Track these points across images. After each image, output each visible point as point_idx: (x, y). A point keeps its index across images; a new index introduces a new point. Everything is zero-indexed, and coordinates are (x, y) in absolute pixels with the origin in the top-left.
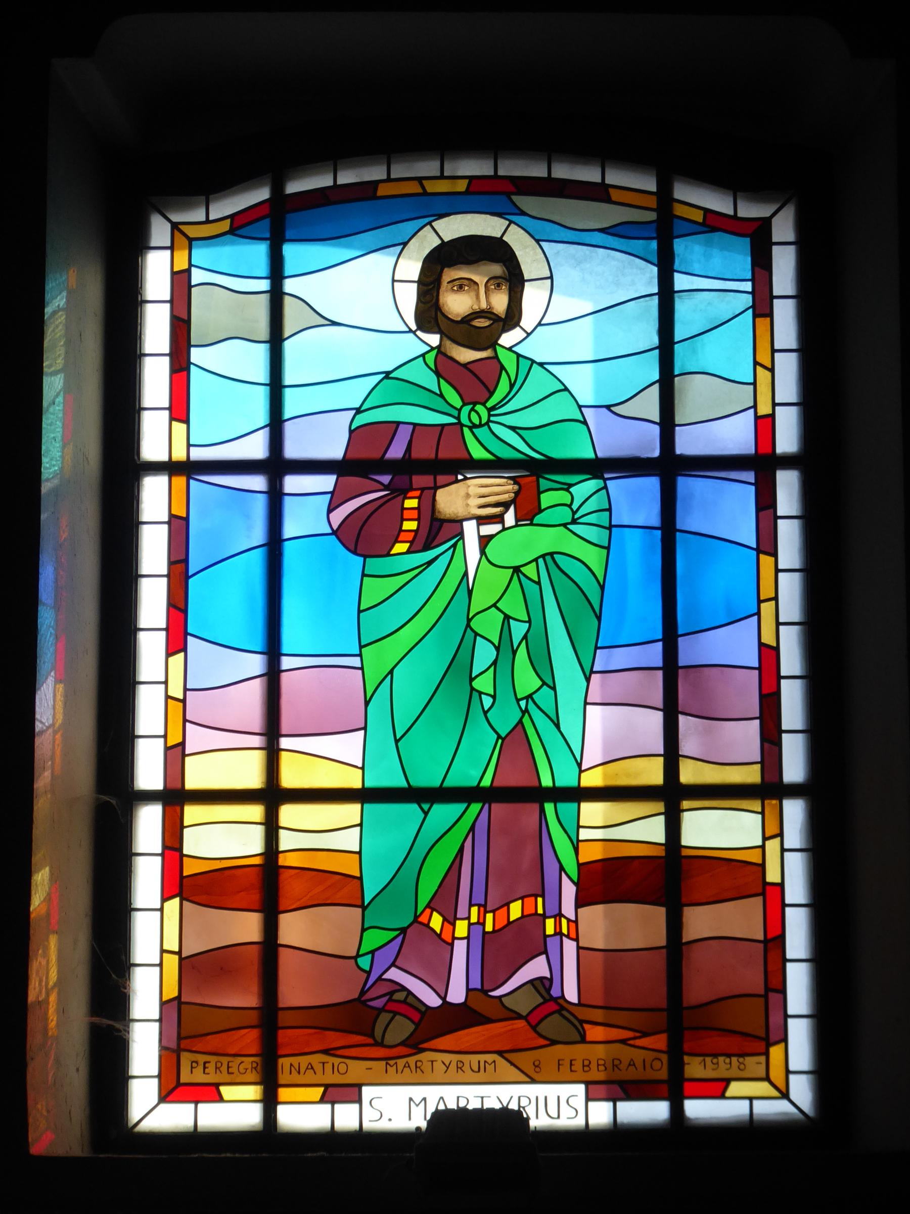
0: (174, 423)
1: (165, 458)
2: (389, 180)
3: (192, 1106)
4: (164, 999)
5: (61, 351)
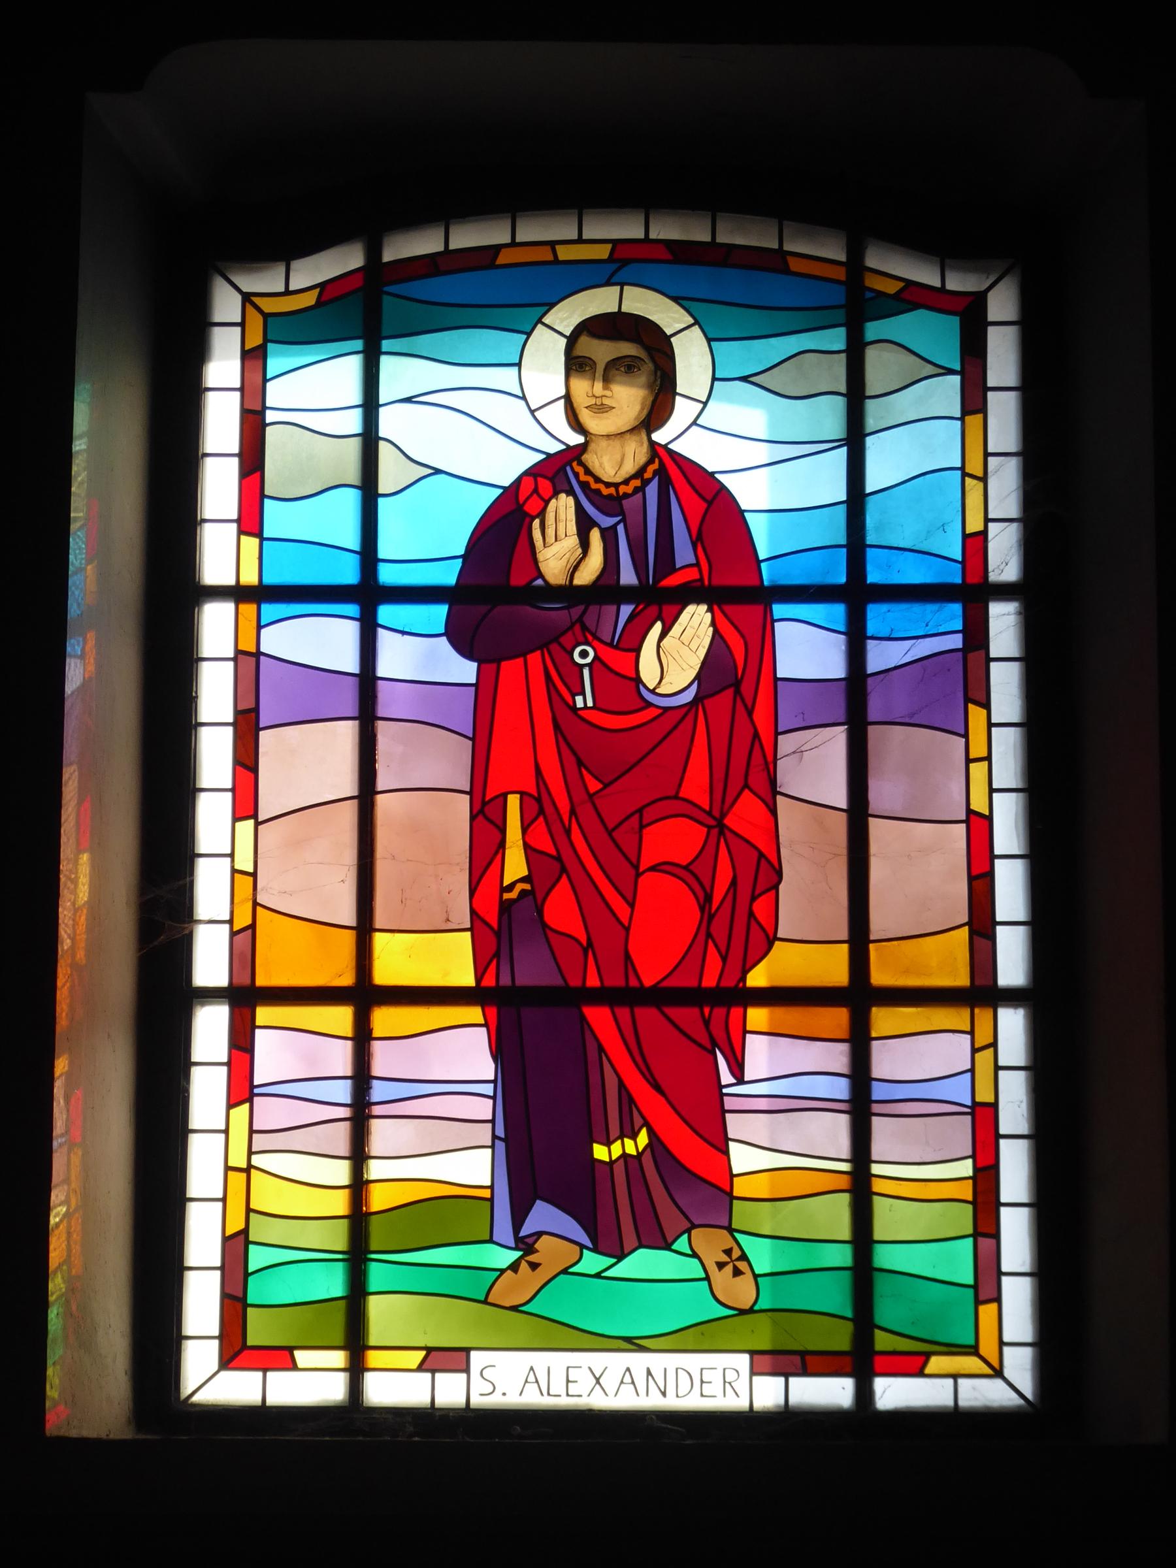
0: (243, 538)
1: (231, 582)
2: (514, 244)
3: (260, 1374)
4: (228, 1233)
5: (72, 840)
